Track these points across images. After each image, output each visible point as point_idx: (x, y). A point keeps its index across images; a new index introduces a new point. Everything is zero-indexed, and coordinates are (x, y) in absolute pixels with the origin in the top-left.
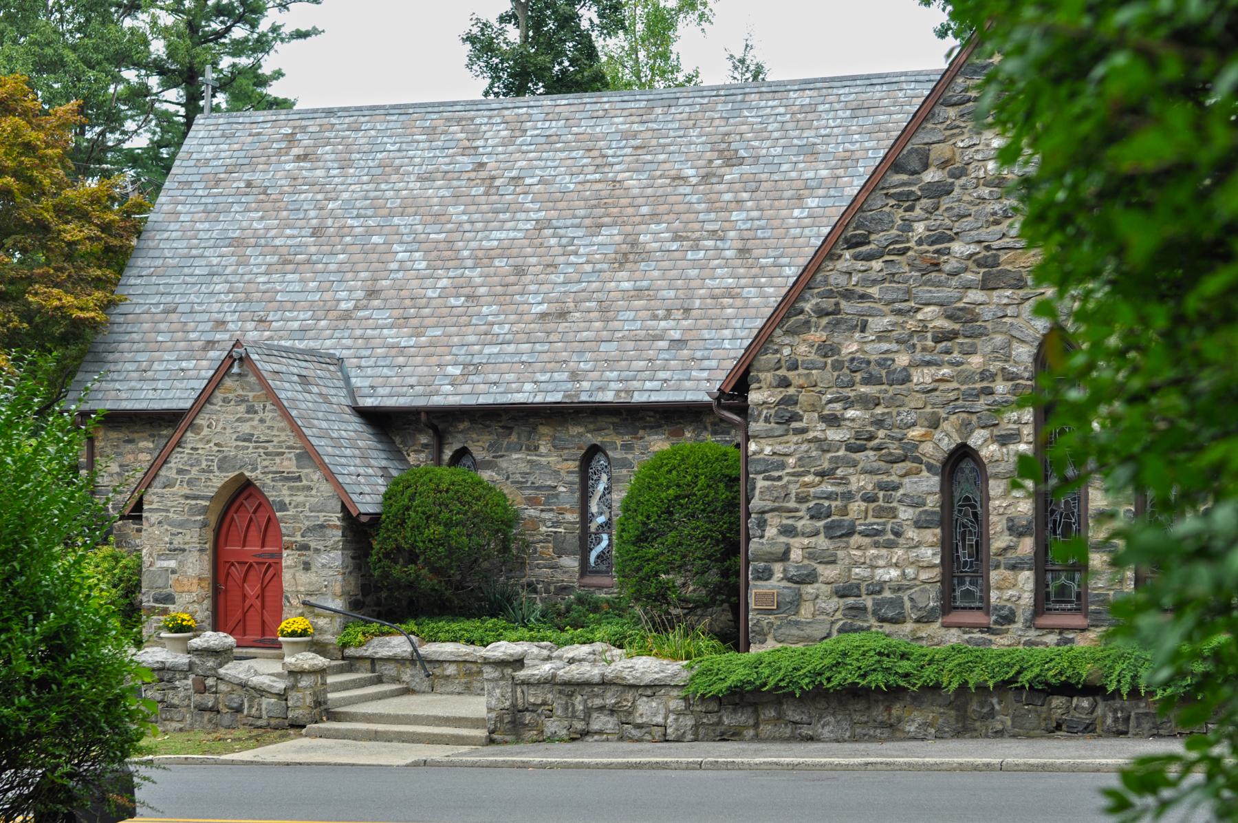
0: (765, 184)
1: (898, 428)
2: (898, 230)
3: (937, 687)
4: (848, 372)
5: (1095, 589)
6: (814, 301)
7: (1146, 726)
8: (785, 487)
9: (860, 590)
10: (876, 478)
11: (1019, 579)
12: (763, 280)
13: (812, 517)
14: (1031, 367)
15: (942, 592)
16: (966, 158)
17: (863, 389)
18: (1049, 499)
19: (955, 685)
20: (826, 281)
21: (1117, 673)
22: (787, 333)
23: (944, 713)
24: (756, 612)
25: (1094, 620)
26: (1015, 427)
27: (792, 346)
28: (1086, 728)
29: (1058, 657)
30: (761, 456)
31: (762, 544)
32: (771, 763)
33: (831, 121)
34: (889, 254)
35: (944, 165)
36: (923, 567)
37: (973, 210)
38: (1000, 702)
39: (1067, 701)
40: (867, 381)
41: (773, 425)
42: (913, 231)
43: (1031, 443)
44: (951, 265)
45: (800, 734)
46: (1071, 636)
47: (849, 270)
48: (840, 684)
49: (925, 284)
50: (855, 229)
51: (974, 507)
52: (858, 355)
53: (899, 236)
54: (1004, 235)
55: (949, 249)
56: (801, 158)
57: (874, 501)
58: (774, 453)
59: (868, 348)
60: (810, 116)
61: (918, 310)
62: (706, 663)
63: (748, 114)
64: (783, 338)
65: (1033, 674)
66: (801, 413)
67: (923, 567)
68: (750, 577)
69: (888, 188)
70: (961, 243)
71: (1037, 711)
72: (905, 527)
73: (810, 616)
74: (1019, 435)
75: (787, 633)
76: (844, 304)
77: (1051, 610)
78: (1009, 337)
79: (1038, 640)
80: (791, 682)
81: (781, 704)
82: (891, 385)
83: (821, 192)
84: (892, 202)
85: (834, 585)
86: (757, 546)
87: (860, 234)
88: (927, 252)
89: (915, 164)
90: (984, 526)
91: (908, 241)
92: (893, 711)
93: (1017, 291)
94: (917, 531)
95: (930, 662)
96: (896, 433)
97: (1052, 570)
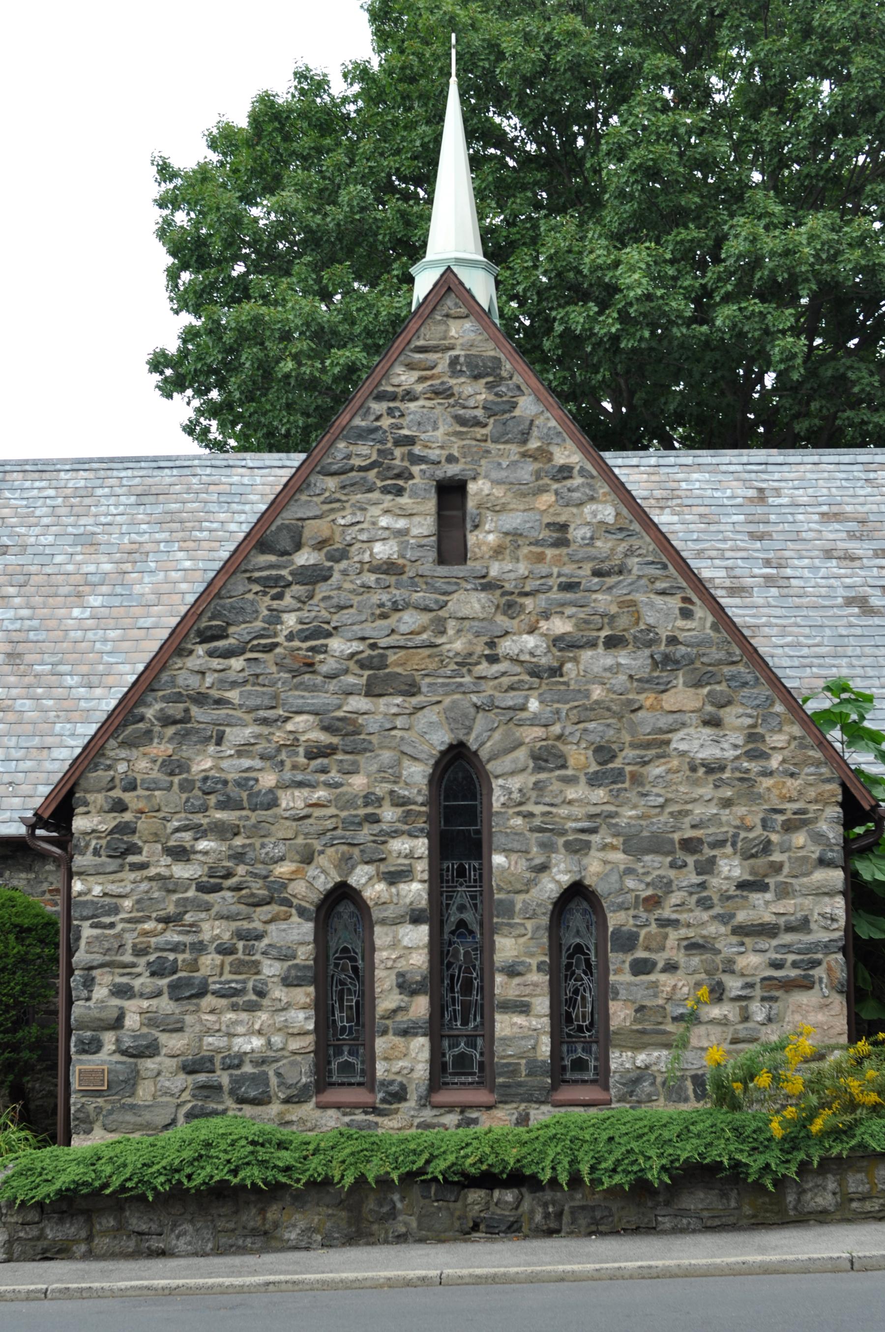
0: (36, 577)
1: (263, 863)
2: (263, 621)
3: (328, 1181)
4: (200, 793)
5: (503, 1057)
6: (158, 706)
7: (583, 1222)
8: (119, 936)
9: (213, 1064)
10: (234, 925)
11: (412, 1046)
12: (40, 691)
13: (153, 974)
14: (425, 790)
15: (316, 1065)
16: (348, 538)
17: (219, 815)
18: (445, 950)
19: (349, 1180)
20: (173, 681)
21: (550, 1158)
22: (123, 744)
23: (333, 1215)
24: (81, 1094)
25: (503, 1095)
26: (407, 862)
27: (129, 761)
28: (509, 1227)
29: (475, 1142)
30: (89, 897)
31: (89, 1008)
32: (141, 1288)
33: (112, 508)
34: (251, 651)
35: (320, 545)
36: (293, 1035)
37: (356, 600)
38: (402, 1199)
39: (487, 1195)
40: (222, 806)
41: (104, 859)
42: (282, 623)
43: (425, 881)
44: (329, 665)
45: (148, 1248)
46: (474, 1115)
47: (202, 669)
48: (204, 1183)
49: (296, 687)
50: (211, 619)
51: (354, 960)
52: (212, 773)
53: (264, 629)
54: (393, 631)
55: (326, 646)
56: (79, 549)
57: (231, 953)
58: (105, 894)
59: (225, 764)
60: (87, 501)
61: (287, 719)
62: (24, 1161)
63: (10, 496)
64: (117, 751)
65: (448, 1163)
66: (140, 844)
67: (293, 1035)
68: (73, 1050)
69: (252, 571)
70: (341, 640)
71: (449, 1209)
72: (270, 985)
73: (149, 1098)
74: (410, 871)
75: (120, 1119)
76: (195, 711)
77: (448, 1084)
78: (398, 754)
79: (435, 1120)
80: (140, 1181)
81: (122, 1209)
82: (254, 810)
83: (105, 589)
84: (256, 588)
85: (181, 1058)
86: (82, 1010)
87: (216, 626)
88: (300, 649)
89: (285, 543)
90: (367, 983)
91: (275, 635)
92: (269, 1215)
93: (408, 699)
94: (285, 989)
95: (316, 1152)
96: (260, 869)
97: (449, 1036)
